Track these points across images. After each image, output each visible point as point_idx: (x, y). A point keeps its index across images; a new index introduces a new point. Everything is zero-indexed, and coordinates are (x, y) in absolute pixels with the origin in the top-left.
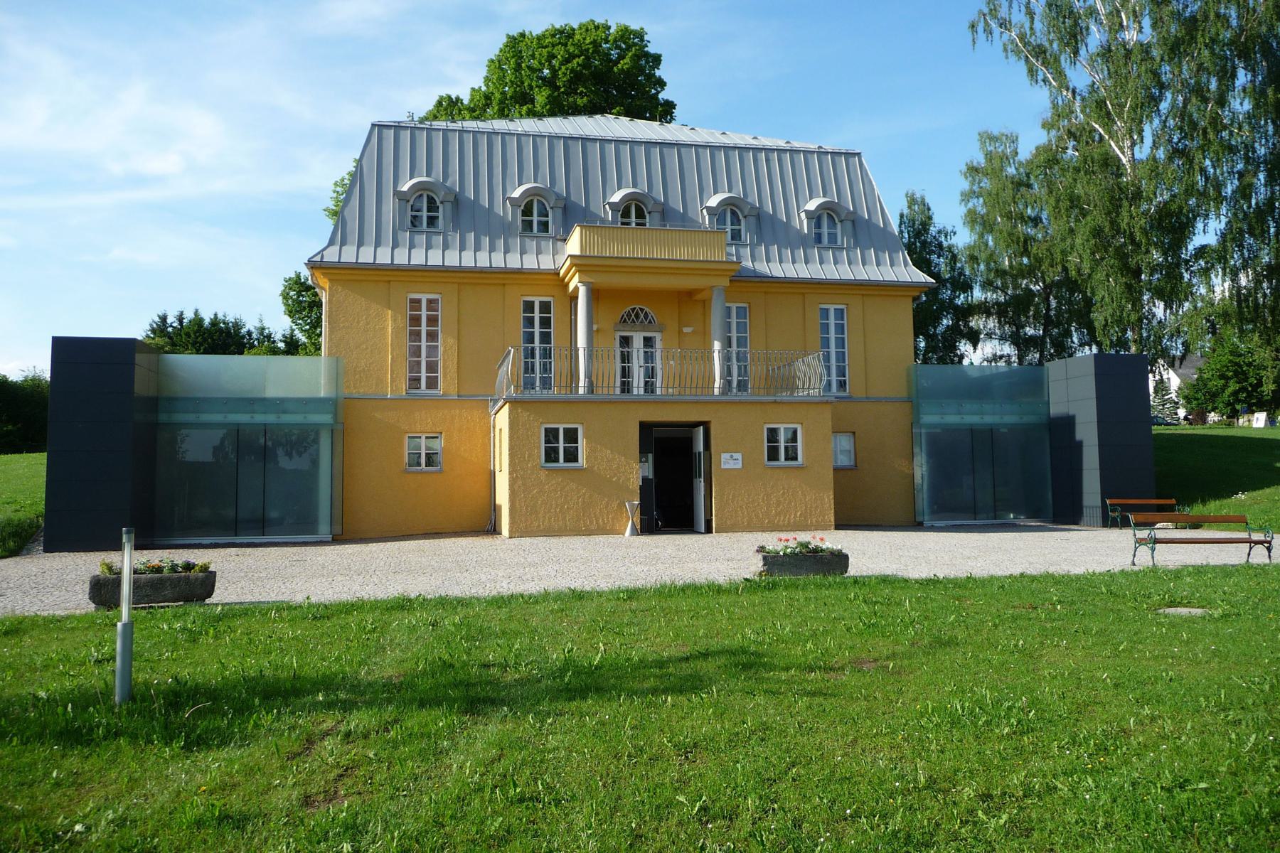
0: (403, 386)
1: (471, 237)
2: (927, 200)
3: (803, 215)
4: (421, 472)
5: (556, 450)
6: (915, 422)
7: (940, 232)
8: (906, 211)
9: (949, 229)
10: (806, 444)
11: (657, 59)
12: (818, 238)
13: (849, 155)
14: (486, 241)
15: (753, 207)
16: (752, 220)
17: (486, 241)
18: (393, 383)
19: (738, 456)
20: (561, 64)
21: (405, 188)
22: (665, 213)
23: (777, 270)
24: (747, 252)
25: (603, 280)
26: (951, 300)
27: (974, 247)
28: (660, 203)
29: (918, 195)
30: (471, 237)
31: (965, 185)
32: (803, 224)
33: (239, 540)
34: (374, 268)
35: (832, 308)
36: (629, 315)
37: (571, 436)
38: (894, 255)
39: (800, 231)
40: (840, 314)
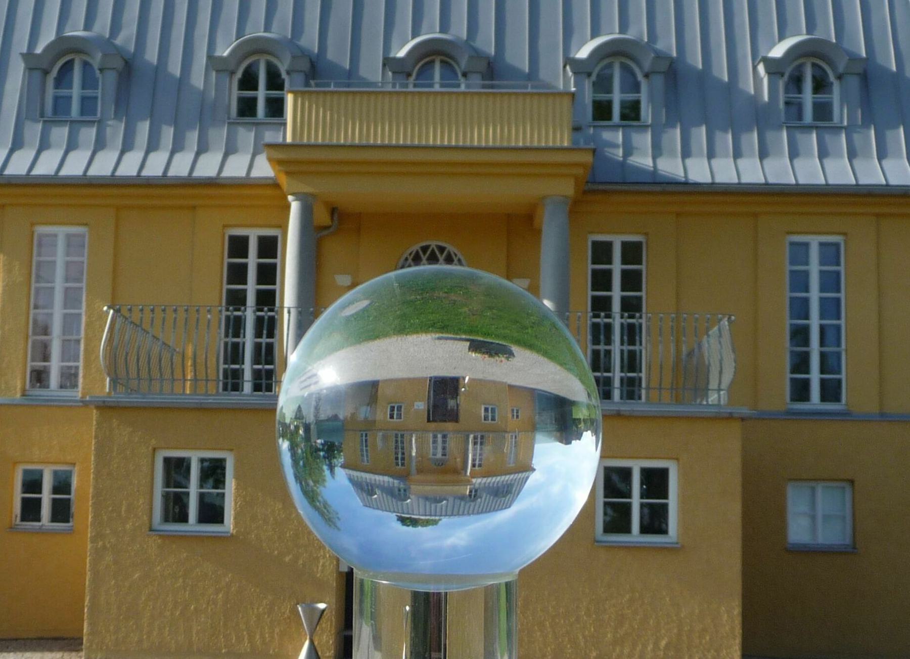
1: (144, 128)
3: (761, 68)
4: (42, 532)
10: (684, 500)
12: (794, 107)
14: (168, 134)
15: (854, 58)
16: (854, 83)
17: (168, 134)
21: (402, 54)
22: (492, 71)
23: (699, 171)
24: (644, 140)
28: (861, 59)
30: (144, 128)
32: (757, 83)
35: (814, 242)
37: (214, 472)
38: (770, 135)
39: (754, 100)
40: (831, 253)
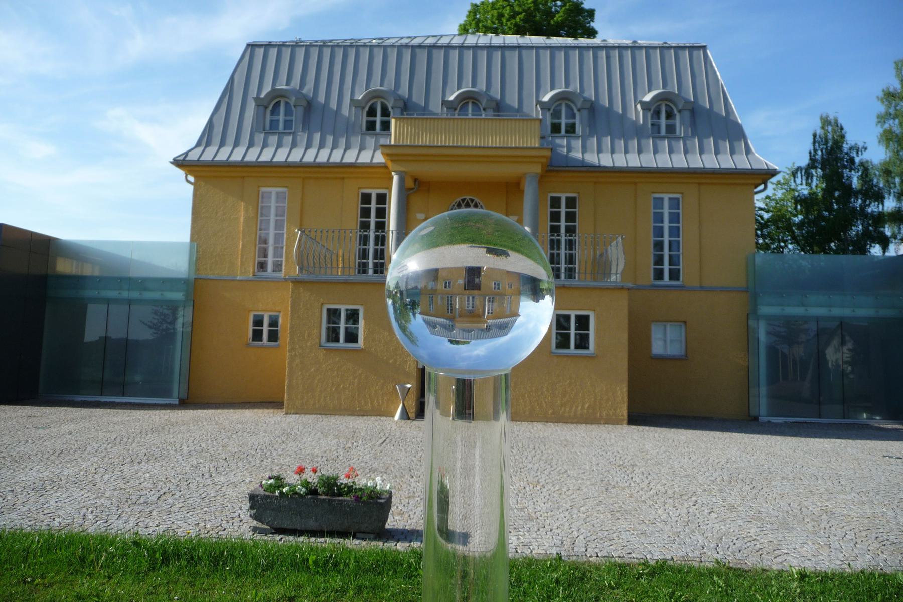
0: (251, 269)
1: (317, 137)
2: (840, 121)
3: (639, 107)
4: (263, 347)
5: (568, 336)
6: (752, 313)
7: (851, 149)
8: (819, 132)
9: (861, 145)
11: (591, 13)
12: (656, 127)
13: (692, 48)
14: (330, 140)
17: (330, 140)
18: (245, 270)
20: (508, 20)
23: (606, 160)
25: (427, 170)
26: (863, 207)
27: (889, 162)
29: (831, 117)
30: (317, 137)
31: (881, 108)
32: (637, 114)
33: (104, 399)
34: (228, 165)
35: (666, 197)
37: (353, 316)
39: (635, 123)
40: (675, 203)
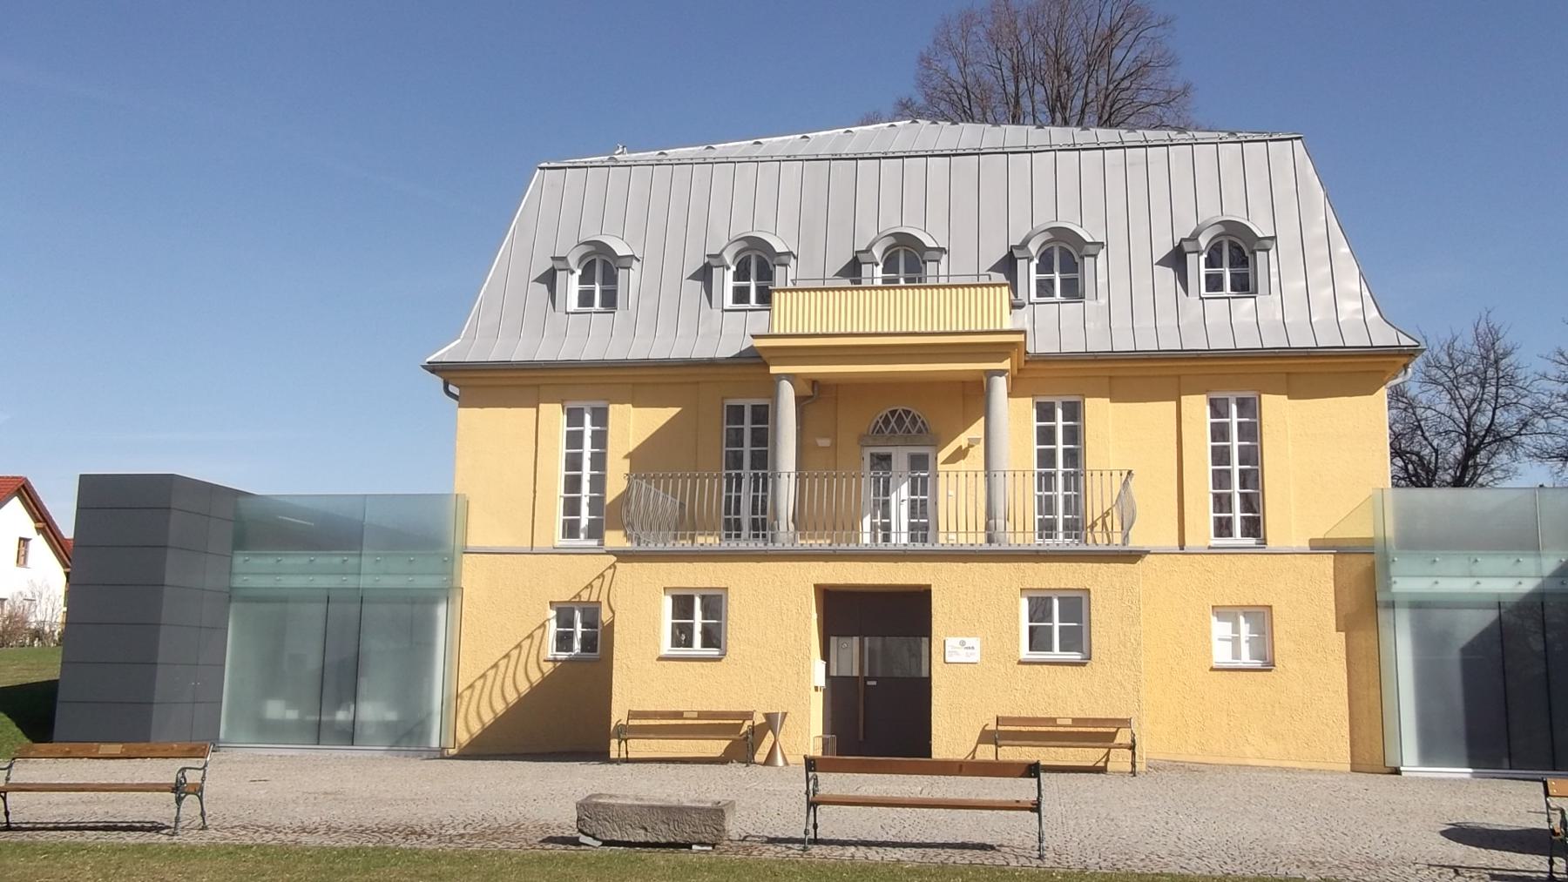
19: (970, 641)
36: (886, 421)
